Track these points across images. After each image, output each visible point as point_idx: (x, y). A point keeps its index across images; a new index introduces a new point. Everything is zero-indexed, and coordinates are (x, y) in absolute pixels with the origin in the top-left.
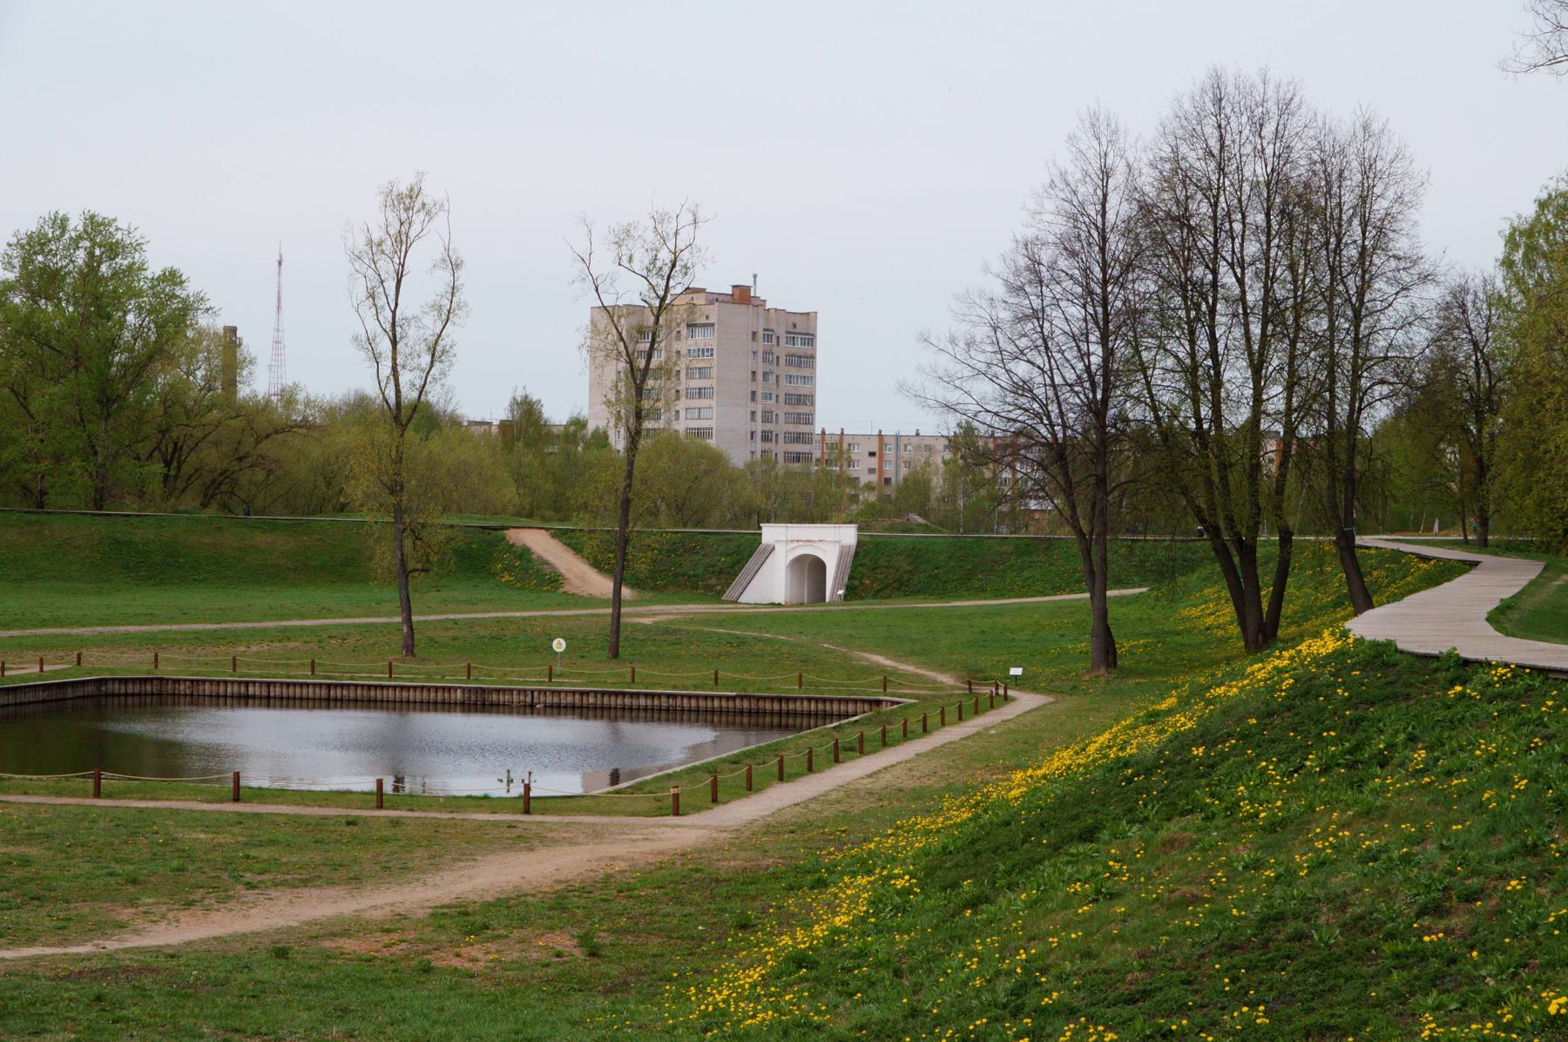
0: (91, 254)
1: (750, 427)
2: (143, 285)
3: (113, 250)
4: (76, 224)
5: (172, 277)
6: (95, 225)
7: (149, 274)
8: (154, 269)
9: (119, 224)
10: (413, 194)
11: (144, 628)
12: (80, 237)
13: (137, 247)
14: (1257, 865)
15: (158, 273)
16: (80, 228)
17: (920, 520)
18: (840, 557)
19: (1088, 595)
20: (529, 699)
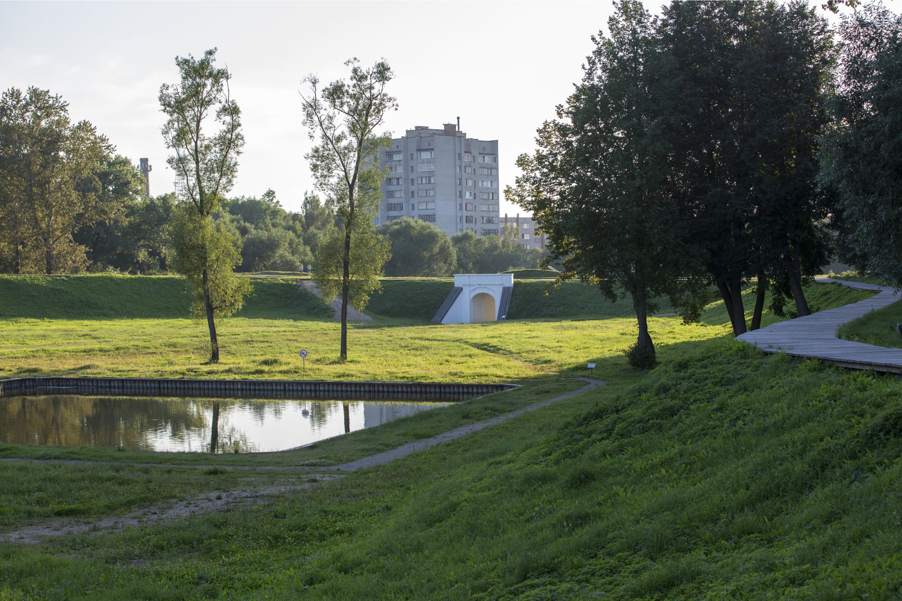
0: (35, 114)
1: (459, 214)
2: (67, 133)
3: (48, 110)
4: (25, 94)
5: (85, 126)
6: (37, 95)
7: (71, 125)
8: (74, 121)
9: (52, 94)
10: (204, 64)
11: (538, 280)
12: (27, 104)
13: (63, 108)
14: (239, 579)
15: (76, 124)
16: (28, 97)
17: (554, 270)
18: (503, 295)
19: (721, 302)
20: (282, 388)
